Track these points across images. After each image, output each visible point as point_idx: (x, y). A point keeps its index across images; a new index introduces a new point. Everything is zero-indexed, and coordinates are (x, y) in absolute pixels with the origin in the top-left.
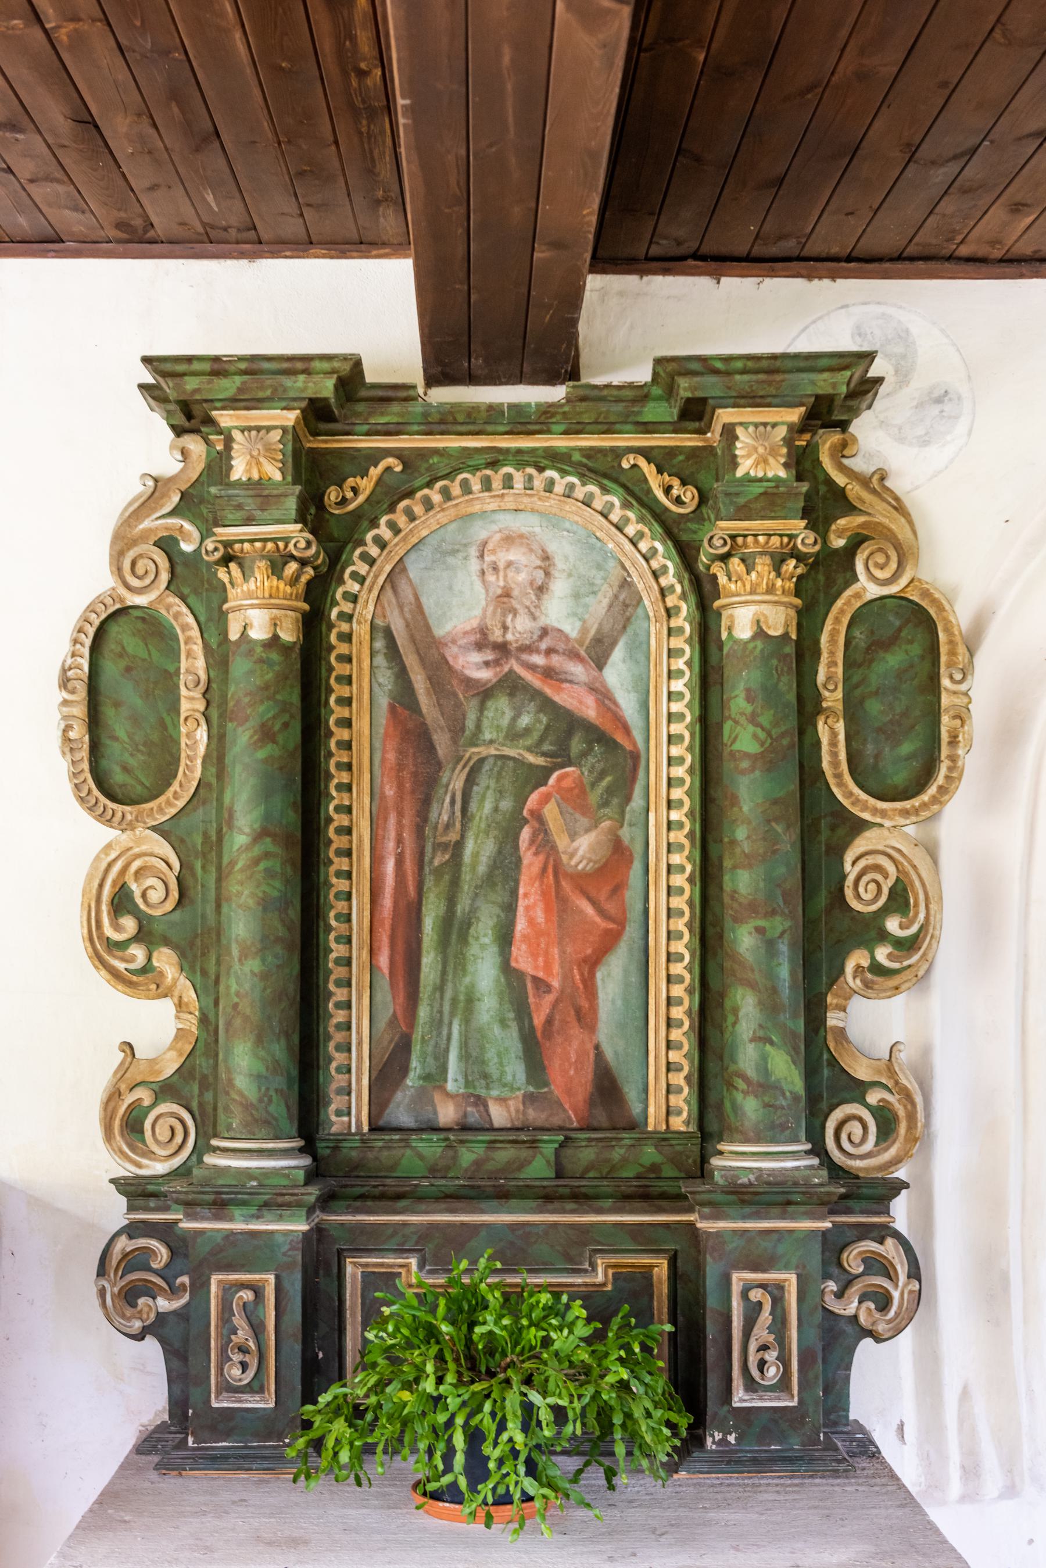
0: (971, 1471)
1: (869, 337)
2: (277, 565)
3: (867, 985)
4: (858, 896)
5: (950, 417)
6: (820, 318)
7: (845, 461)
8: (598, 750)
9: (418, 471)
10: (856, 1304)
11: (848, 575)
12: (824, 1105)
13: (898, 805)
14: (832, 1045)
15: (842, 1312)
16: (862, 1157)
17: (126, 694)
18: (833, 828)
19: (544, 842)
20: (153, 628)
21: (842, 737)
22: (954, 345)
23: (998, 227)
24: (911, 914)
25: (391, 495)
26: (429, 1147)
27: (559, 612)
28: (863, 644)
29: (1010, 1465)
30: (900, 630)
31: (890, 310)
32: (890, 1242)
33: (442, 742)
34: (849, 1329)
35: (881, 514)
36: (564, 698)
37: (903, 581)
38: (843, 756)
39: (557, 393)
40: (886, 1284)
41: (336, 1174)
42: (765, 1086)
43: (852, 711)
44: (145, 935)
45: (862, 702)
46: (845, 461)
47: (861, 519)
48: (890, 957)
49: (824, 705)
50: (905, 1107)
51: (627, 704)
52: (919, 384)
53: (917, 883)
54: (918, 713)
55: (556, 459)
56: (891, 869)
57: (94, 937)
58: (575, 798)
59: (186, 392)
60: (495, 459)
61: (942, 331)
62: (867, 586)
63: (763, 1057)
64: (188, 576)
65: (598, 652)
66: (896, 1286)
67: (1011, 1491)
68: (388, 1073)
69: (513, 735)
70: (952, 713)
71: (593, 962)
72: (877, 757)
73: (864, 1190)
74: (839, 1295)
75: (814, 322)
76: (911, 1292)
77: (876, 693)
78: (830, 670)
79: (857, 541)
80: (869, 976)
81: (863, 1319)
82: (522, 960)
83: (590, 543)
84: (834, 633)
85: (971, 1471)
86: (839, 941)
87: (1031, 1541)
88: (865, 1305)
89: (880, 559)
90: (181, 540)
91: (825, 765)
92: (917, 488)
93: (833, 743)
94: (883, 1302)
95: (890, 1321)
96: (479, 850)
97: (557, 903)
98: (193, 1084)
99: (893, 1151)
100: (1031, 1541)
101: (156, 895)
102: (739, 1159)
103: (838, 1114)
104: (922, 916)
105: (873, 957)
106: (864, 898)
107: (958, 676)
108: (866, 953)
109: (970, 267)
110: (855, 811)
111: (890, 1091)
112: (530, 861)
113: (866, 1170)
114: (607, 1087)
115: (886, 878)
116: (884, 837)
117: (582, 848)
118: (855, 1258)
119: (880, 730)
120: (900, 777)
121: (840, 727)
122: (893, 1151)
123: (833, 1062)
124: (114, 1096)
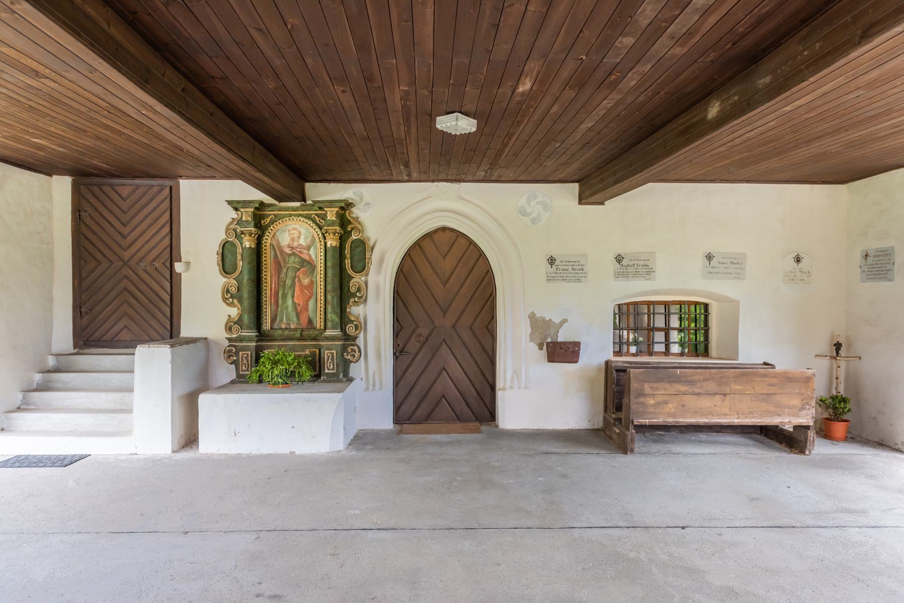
0: (374, 386)
2: (250, 235)
8: (308, 265)
9: (277, 218)
17: (228, 256)
19: (299, 281)
20: (233, 244)
23: (353, 176)
25: (272, 222)
26: (280, 332)
27: (302, 241)
29: (381, 385)
33: (282, 264)
35: (356, 224)
36: (303, 256)
39: (298, 204)
41: (262, 336)
42: (333, 321)
43: (351, 258)
44: (232, 297)
51: (313, 257)
52: (364, 202)
55: (295, 215)
57: (223, 297)
58: (305, 273)
59: (236, 205)
60: (290, 216)
62: (354, 237)
63: (333, 317)
64: (237, 236)
65: (309, 248)
68: (273, 320)
69: (294, 263)
71: (308, 301)
78: (347, 252)
79: (352, 229)
82: (296, 300)
83: (307, 229)
85: (374, 386)
90: (235, 230)
94: (354, 356)
96: (289, 282)
97: (302, 290)
98: (239, 322)
101: (233, 290)
102: (329, 333)
106: (353, 290)
112: (297, 284)
114: (310, 322)
116: (357, 280)
117: (306, 282)
124: (227, 324)
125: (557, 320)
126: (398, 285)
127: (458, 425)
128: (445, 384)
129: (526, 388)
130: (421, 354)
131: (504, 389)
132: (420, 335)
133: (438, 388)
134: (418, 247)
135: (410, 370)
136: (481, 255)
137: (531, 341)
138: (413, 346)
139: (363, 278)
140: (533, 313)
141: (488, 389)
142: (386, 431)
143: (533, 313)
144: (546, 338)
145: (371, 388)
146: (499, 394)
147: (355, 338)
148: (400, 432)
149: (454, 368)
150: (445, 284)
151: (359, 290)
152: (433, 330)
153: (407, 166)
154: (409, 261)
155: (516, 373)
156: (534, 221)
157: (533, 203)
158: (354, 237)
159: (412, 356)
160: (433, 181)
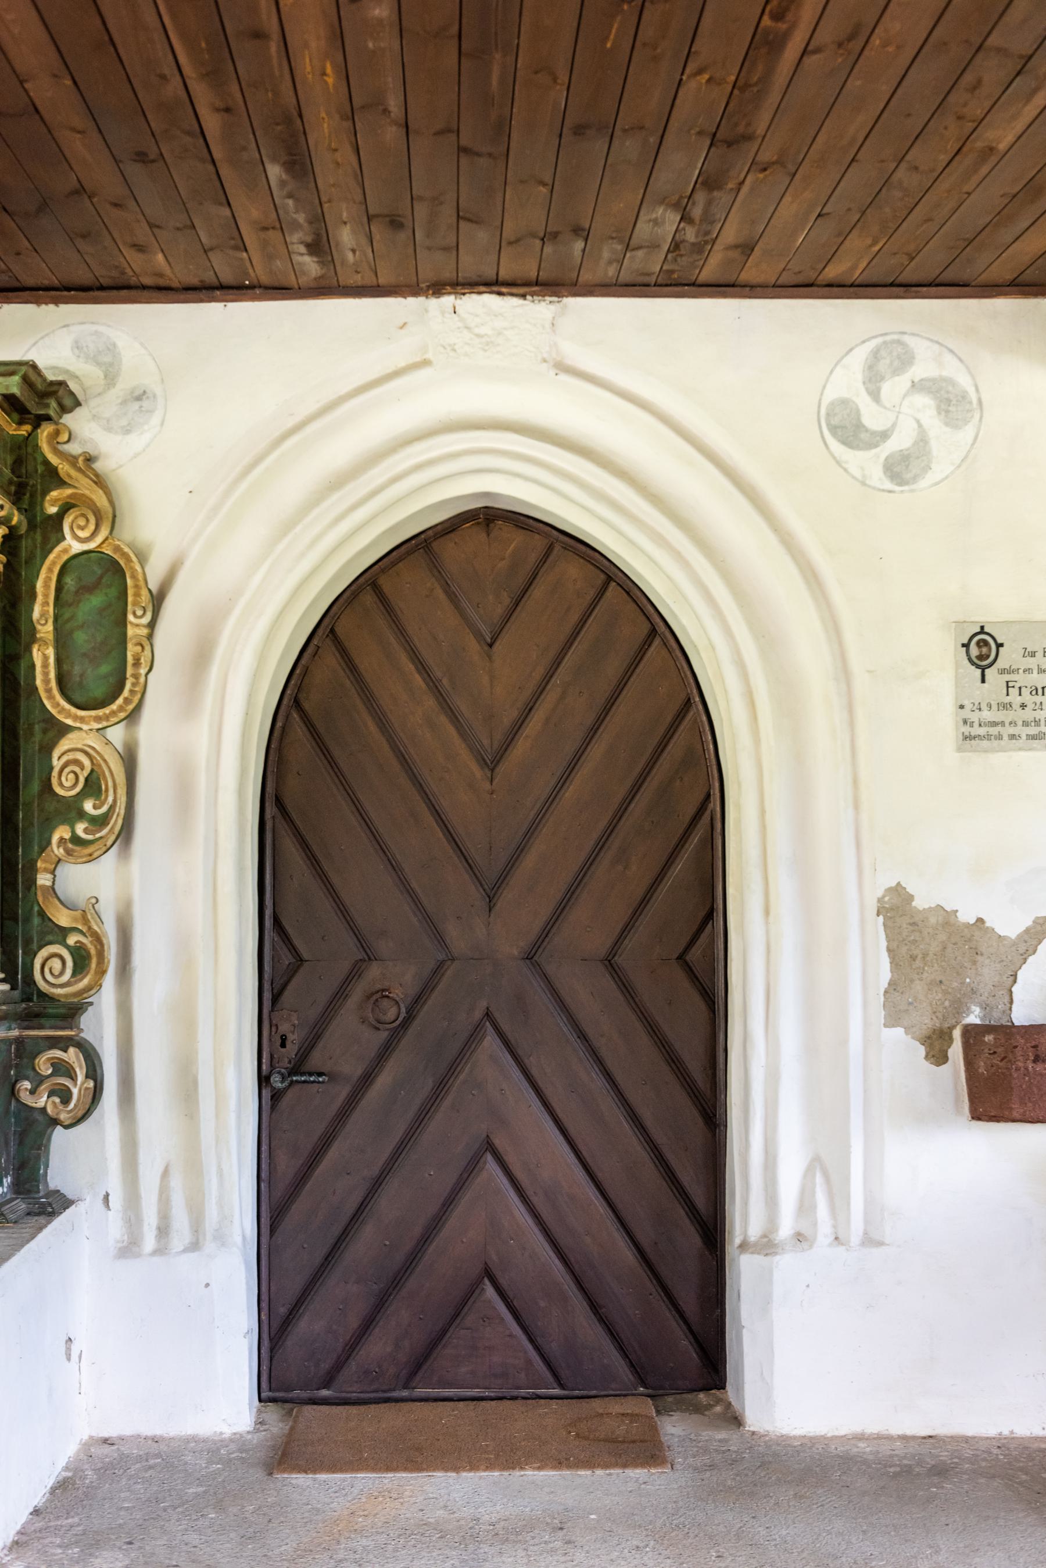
0: (163, 1231)
1: (85, 349)
3: (69, 852)
4: (61, 785)
5: (147, 411)
6: (47, 335)
7: (60, 447)
10: (45, 1098)
11: (60, 535)
12: (35, 946)
13: (93, 713)
14: (40, 900)
15: (34, 1105)
16: (62, 986)
18: (45, 731)
21: (52, 660)
22: (151, 355)
24: (103, 797)
28: (73, 589)
30: (101, 578)
31: (101, 329)
32: (72, 1050)
34: (40, 1118)
35: (85, 487)
37: (99, 539)
38: (52, 675)
40: (67, 1082)
43: (62, 641)
45: (71, 632)
46: (60, 447)
47: (69, 491)
48: (86, 831)
49: (38, 636)
50: (96, 947)
53: (107, 773)
54: (114, 641)
56: (87, 762)
61: (142, 344)
62: (72, 545)
66: (76, 1085)
67: (195, 1246)
70: (134, 641)
72: (81, 676)
73: (50, 1011)
74: (33, 1092)
75: (42, 338)
76: (87, 1089)
77: (82, 626)
79: (66, 508)
80: (70, 846)
81: (49, 1110)
84: (48, 579)
86: (47, 819)
87: (207, 1285)
88: (51, 1099)
89: (82, 522)
91: (39, 682)
92: (121, 466)
93: (45, 665)
94: (65, 1096)
95: (71, 1111)
99: (86, 982)
100: (207, 1285)
103: (43, 953)
104: (110, 799)
105: (73, 832)
106: (65, 786)
107: (139, 613)
108: (67, 828)
109: (155, 294)
110: (61, 718)
111: (84, 934)
113: (66, 996)
115: (82, 769)
118: (44, 1063)
119: (85, 655)
120: (99, 692)
121: (51, 652)
122: (86, 982)
123: (42, 914)
125: (1009, 924)
126: (281, 761)
127: (553, 1415)
128: (495, 1221)
129: (870, 1241)
130: (384, 1080)
131: (767, 1246)
132: (383, 994)
133: (462, 1238)
134: (368, 598)
135: (333, 1154)
136: (655, 633)
137: (893, 1019)
138: (348, 1044)
139: (117, 734)
140: (898, 890)
141: (691, 1239)
142: (212, 1448)
143: (898, 890)
144: (959, 1008)
145: (149, 1242)
146: (745, 1272)
147: (71, 1012)
148: (285, 1456)
149: (533, 1158)
150: (491, 763)
151: (93, 786)
152: (439, 969)
153: (299, 163)
154: (330, 659)
155: (825, 1170)
156: (901, 470)
157: (893, 388)
158: (72, 545)
159: (342, 1092)
160: (437, 288)
